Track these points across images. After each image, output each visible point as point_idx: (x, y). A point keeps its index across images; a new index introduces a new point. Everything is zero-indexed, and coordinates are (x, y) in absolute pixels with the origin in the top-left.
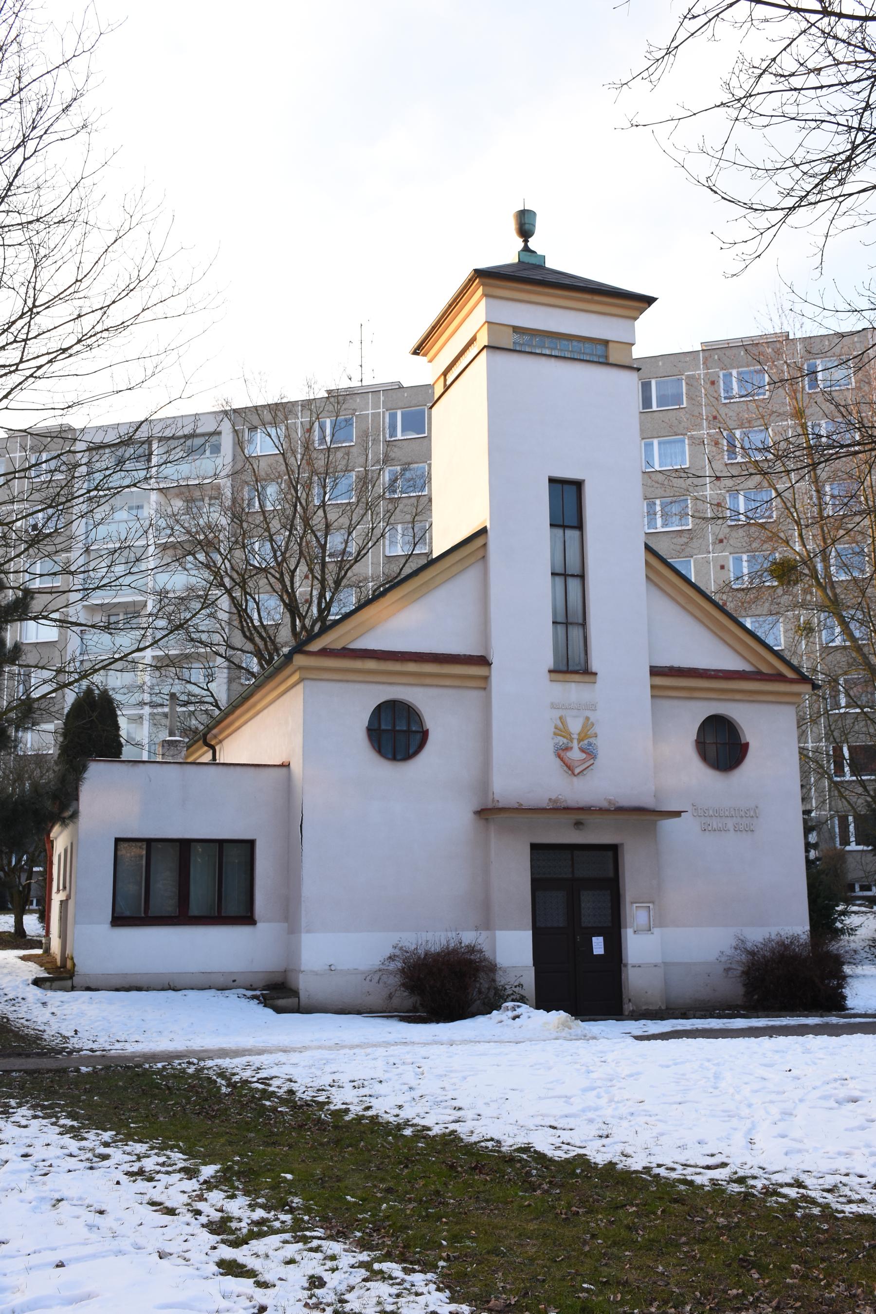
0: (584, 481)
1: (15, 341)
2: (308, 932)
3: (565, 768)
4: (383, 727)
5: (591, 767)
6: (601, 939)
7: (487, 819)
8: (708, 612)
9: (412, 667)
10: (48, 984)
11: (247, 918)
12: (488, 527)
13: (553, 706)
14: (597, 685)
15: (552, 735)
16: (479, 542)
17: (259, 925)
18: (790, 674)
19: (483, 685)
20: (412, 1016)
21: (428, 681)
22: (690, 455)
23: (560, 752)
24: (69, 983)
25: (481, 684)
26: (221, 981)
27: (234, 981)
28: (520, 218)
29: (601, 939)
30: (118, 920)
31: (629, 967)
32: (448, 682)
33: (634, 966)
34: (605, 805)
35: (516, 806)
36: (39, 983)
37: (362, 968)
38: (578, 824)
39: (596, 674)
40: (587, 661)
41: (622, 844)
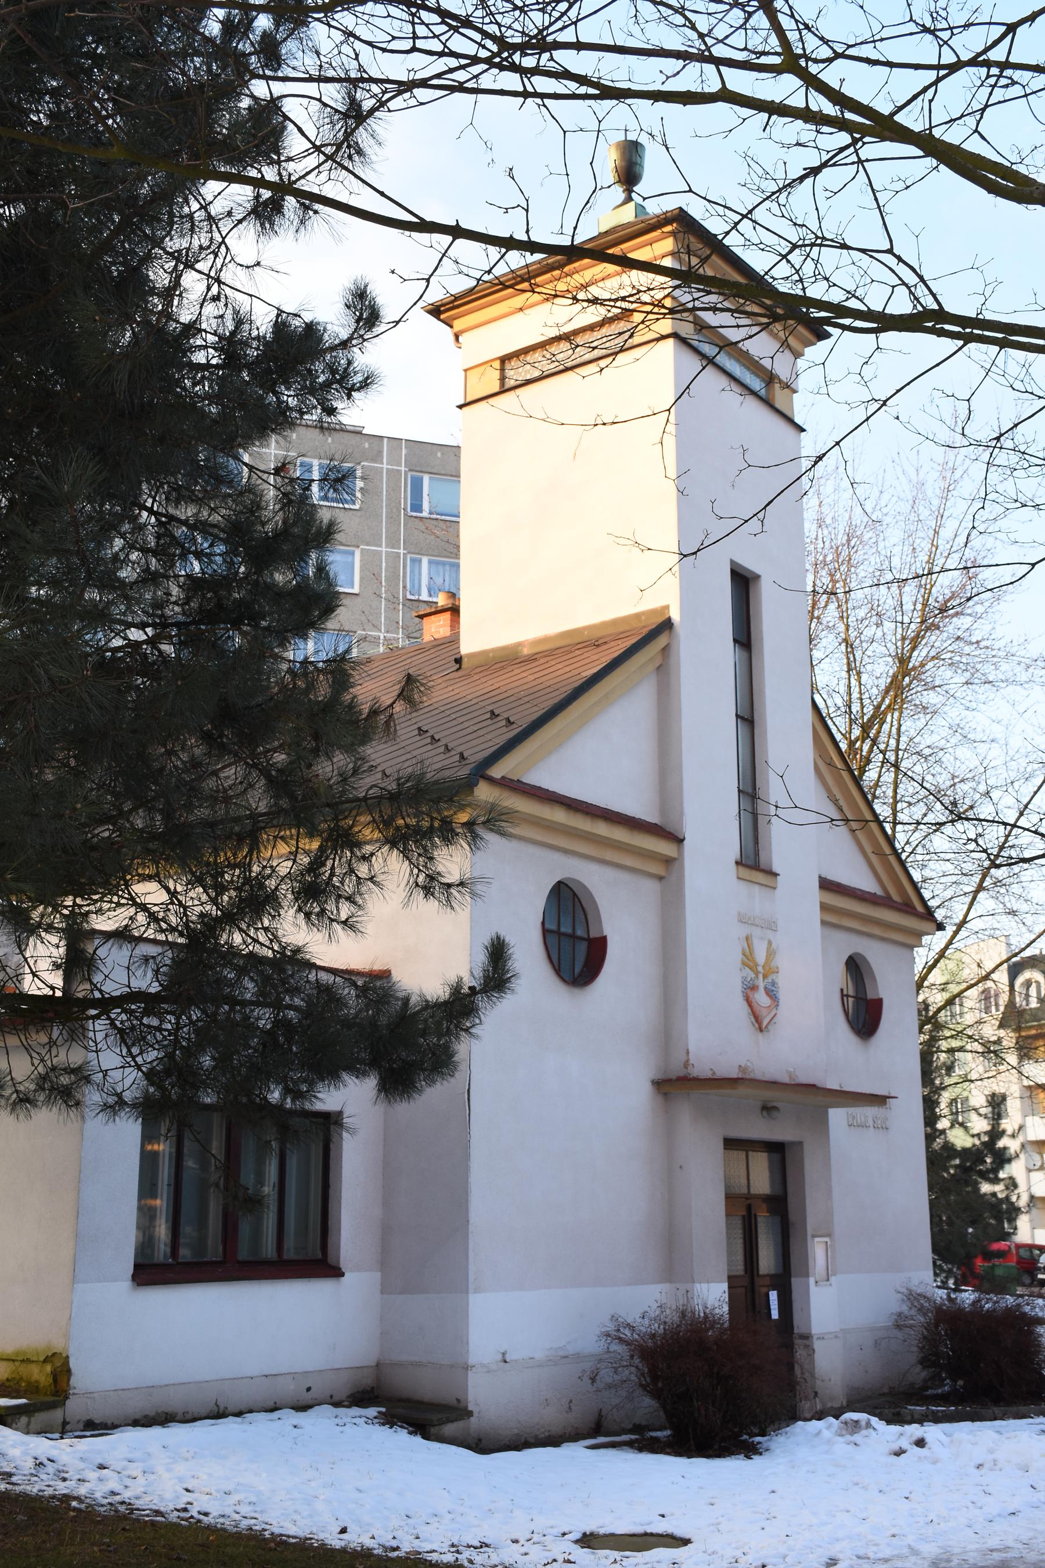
0: (758, 577)
1: (701, 36)
2: (476, 1291)
3: (753, 1020)
4: (563, 930)
5: (775, 1020)
6: (775, 1293)
7: (665, 1094)
8: (854, 799)
9: (602, 829)
10: (24, 1420)
11: (319, 1263)
12: (675, 615)
13: (742, 920)
14: (778, 891)
15: (739, 965)
16: (662, 641)
17: (349, 1278)
18: (920, 908)
19: (662, 873)
20: (643, 1442)
21: (609, 855)
22: (362, 570)
23: (749, 991)
24: (57, 1415)
25: (657, 869)
26: (290, 1389)
27: (309, 1389)
28: (630, 152)
29: (775, 1293)
30: (149, 1272)
31: (815, 1338)
32: (628, 861)
33: (819, 1338)
34: (786, 1080)
35: (709, 1075)
36: (9, 1420)
37: (539, 1355)
38: (768, 1109)
39: (776, 875)
40: (757, 853)
41: (801, 1143)
